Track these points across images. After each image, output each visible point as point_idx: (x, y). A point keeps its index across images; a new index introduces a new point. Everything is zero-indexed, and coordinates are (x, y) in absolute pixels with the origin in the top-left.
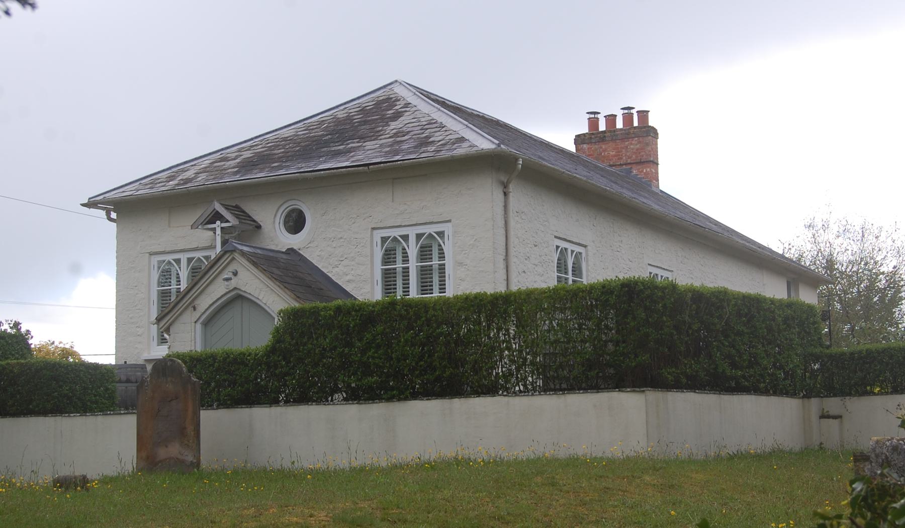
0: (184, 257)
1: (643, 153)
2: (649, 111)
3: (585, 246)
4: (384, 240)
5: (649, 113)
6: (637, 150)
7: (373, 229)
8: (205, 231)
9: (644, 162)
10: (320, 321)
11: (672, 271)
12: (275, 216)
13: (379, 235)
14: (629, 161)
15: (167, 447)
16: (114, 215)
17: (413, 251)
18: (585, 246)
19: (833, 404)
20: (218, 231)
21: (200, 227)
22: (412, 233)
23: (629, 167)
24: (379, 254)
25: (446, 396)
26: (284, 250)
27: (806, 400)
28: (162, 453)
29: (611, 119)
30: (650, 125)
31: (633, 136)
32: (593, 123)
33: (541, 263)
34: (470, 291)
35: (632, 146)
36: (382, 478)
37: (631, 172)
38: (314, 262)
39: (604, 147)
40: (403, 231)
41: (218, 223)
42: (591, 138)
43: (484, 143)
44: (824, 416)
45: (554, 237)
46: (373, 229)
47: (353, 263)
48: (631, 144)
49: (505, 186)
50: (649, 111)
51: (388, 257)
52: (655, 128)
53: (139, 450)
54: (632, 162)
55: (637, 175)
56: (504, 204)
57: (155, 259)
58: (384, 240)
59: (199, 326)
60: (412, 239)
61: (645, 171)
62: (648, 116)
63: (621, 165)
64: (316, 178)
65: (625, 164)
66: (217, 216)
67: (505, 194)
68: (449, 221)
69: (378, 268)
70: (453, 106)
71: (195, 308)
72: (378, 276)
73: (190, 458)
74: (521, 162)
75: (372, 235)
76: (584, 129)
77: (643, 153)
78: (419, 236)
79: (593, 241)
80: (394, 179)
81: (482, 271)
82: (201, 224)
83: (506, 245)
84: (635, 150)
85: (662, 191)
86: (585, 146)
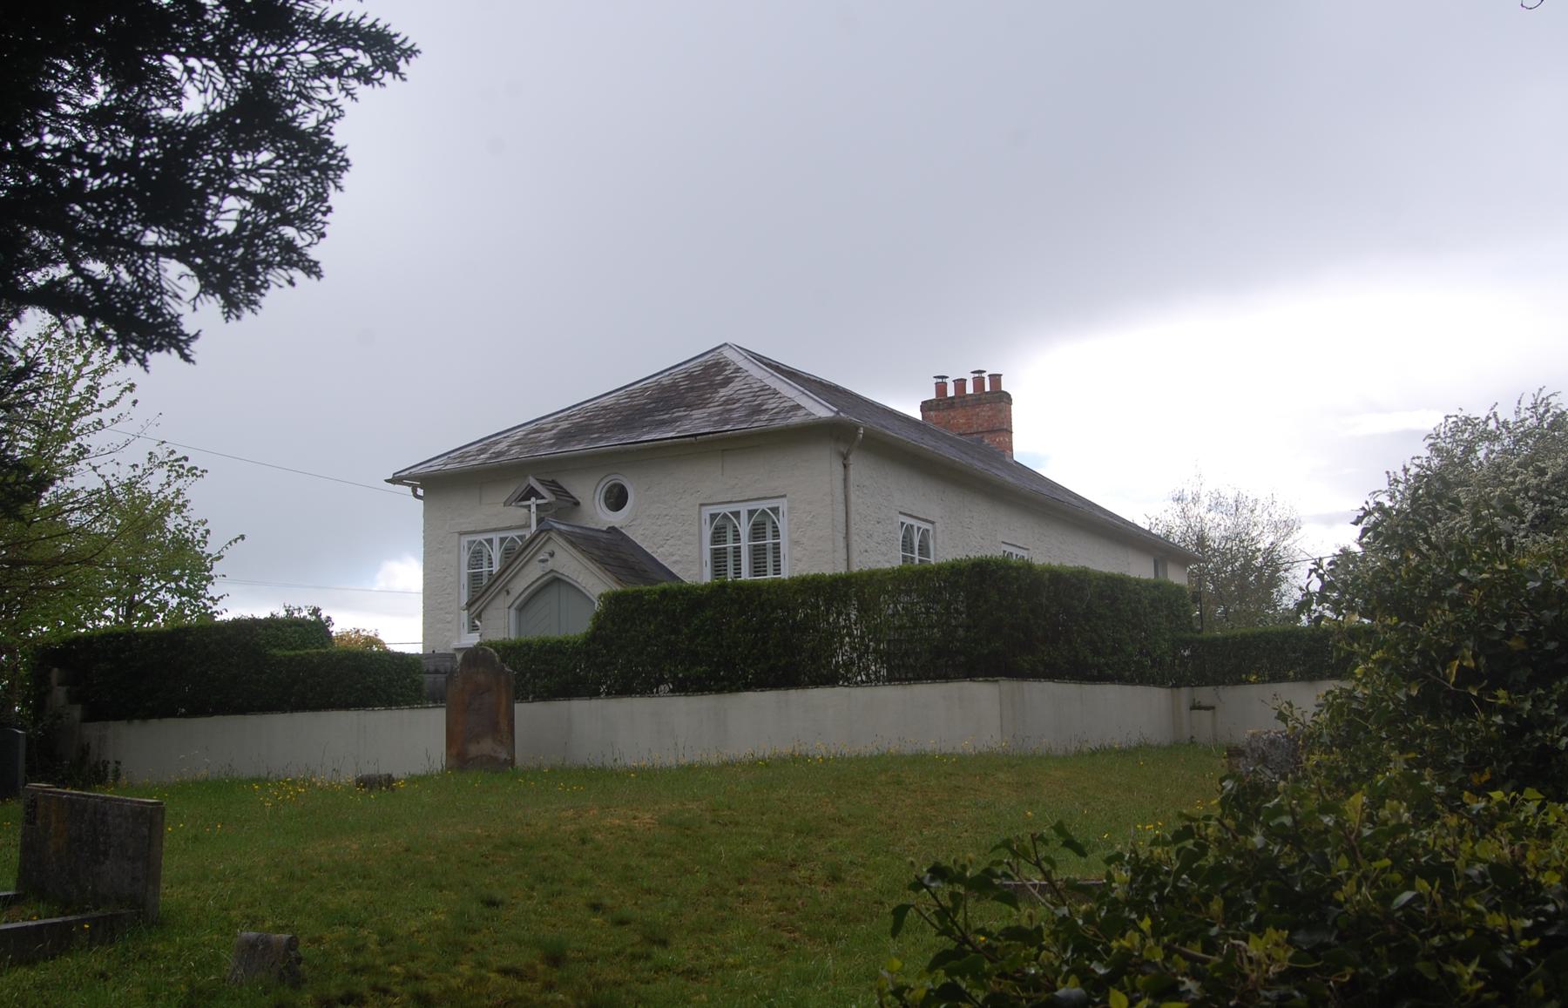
0: (496, 537)
4: (713, 517)
7: (702, 505)
12: (595, 491)
13: (707, 512)
14: (980, 429)
15: (478, 743)
16: (420, 492)
17: (745, 529)
18: (933, 523)
19: (1205, 694)
20: (533, 509)
22: (744, 509)
23: (979, 436)
24: (708, 532)
26: (605, 529)
27: (1175, 690)
28: (473, 750)
29: (960, 384)
30: (1003, 389)
32: (941, 388)
39: (952, 414)
40: (734, 508)
41: (533, 499)
42: (938, 405)
43: (821, 411)
46: (702, 505)
47: (680, 542)
49: (845, 457)
51: (718, 535)
53: (448, 747)
57: (465, 540)
58: (713, 517)
59: (513, 612)
60: (744, 516)
64: (639, 450)
65: (977, 433)
66: (531, 493)
67: (845, 466)
68: (784, 496)
69: (707, 547)
71: (508, 593)
72: (707, 556)
73: (504, 755)
75: (700, 512)
76: (932, 396)
78: (751, 513)
80: (723, 450)
81: (819, 551)
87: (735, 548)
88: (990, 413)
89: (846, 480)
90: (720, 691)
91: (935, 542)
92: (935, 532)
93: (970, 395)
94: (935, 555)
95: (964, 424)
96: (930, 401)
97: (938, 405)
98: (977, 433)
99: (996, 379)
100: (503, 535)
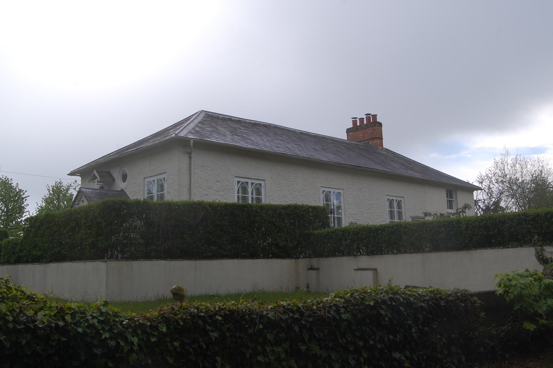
1: (373, 134)
2: (377, 115)
3: (264, 180)
5: (377, 116)
6: (371, 133)
7: (145, 178)
8: (93, 183)
9: (374, 138)
10: (132, 221)
11: (343, 189)
12: (119, 174)
13: (236, 180)
14: (368, 139)
18: (264, 180)
19: (315, 262)
21: (91, 181)
23: (368, 141)
25: (72, 261)
26: (120, 190)
27: (297, 260)
29: (362, 120)
30: (378, 121)
31: (369, 127)
32: (354, 122)
33: (222, 190)
34: (295, 202)
35: (369, 132)
36: (549, 270)
37: (369, 143)
38: (128, 194)
39: (358, 133)
42: (352, 129)
44: (311, 269)
45: (234, 177)
46: (145, 178)
48: (369, 130)
49: (190, 154)
50: (377, 115)
52: (380, 122)
54: (369, 139)
55: (371, 144)
56: (189, 163)
61: (374, 142)
62: (376, 117)
63: (365, 140)
65: (367, 140)
67: (190, 158)
68: (166, 173)
70: (249, 122)
74: (192, 142)
75: (144, 181)
76: (351, 126)
77: (373, 134)
79: (271, 178)
82: (91, 180)
83: (190, 183)
84: (370, 133)
85: (387, 150)
86: (350, 133)
87: (239, 194)
88: (371, 131)
89: (190, 164)
90: (195, 259)
91: (265, 189)
92: (265, 185)
93: (365, 124)
94: (265, 194)
95: (362, 137)
96: (350, 128)
97: (352, 129)
98: (367, 140)
99: (375, 116)
100: (324, 189)
